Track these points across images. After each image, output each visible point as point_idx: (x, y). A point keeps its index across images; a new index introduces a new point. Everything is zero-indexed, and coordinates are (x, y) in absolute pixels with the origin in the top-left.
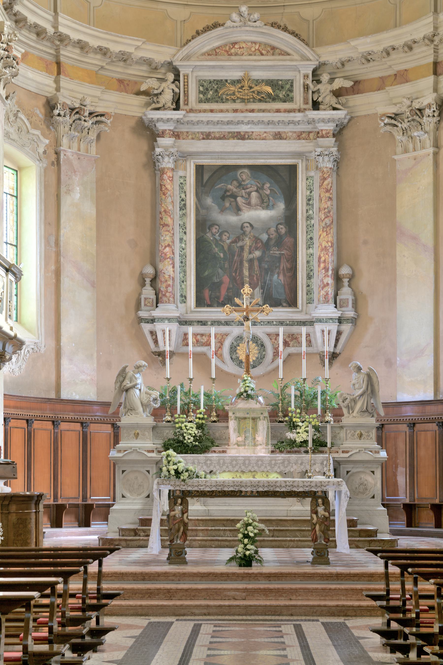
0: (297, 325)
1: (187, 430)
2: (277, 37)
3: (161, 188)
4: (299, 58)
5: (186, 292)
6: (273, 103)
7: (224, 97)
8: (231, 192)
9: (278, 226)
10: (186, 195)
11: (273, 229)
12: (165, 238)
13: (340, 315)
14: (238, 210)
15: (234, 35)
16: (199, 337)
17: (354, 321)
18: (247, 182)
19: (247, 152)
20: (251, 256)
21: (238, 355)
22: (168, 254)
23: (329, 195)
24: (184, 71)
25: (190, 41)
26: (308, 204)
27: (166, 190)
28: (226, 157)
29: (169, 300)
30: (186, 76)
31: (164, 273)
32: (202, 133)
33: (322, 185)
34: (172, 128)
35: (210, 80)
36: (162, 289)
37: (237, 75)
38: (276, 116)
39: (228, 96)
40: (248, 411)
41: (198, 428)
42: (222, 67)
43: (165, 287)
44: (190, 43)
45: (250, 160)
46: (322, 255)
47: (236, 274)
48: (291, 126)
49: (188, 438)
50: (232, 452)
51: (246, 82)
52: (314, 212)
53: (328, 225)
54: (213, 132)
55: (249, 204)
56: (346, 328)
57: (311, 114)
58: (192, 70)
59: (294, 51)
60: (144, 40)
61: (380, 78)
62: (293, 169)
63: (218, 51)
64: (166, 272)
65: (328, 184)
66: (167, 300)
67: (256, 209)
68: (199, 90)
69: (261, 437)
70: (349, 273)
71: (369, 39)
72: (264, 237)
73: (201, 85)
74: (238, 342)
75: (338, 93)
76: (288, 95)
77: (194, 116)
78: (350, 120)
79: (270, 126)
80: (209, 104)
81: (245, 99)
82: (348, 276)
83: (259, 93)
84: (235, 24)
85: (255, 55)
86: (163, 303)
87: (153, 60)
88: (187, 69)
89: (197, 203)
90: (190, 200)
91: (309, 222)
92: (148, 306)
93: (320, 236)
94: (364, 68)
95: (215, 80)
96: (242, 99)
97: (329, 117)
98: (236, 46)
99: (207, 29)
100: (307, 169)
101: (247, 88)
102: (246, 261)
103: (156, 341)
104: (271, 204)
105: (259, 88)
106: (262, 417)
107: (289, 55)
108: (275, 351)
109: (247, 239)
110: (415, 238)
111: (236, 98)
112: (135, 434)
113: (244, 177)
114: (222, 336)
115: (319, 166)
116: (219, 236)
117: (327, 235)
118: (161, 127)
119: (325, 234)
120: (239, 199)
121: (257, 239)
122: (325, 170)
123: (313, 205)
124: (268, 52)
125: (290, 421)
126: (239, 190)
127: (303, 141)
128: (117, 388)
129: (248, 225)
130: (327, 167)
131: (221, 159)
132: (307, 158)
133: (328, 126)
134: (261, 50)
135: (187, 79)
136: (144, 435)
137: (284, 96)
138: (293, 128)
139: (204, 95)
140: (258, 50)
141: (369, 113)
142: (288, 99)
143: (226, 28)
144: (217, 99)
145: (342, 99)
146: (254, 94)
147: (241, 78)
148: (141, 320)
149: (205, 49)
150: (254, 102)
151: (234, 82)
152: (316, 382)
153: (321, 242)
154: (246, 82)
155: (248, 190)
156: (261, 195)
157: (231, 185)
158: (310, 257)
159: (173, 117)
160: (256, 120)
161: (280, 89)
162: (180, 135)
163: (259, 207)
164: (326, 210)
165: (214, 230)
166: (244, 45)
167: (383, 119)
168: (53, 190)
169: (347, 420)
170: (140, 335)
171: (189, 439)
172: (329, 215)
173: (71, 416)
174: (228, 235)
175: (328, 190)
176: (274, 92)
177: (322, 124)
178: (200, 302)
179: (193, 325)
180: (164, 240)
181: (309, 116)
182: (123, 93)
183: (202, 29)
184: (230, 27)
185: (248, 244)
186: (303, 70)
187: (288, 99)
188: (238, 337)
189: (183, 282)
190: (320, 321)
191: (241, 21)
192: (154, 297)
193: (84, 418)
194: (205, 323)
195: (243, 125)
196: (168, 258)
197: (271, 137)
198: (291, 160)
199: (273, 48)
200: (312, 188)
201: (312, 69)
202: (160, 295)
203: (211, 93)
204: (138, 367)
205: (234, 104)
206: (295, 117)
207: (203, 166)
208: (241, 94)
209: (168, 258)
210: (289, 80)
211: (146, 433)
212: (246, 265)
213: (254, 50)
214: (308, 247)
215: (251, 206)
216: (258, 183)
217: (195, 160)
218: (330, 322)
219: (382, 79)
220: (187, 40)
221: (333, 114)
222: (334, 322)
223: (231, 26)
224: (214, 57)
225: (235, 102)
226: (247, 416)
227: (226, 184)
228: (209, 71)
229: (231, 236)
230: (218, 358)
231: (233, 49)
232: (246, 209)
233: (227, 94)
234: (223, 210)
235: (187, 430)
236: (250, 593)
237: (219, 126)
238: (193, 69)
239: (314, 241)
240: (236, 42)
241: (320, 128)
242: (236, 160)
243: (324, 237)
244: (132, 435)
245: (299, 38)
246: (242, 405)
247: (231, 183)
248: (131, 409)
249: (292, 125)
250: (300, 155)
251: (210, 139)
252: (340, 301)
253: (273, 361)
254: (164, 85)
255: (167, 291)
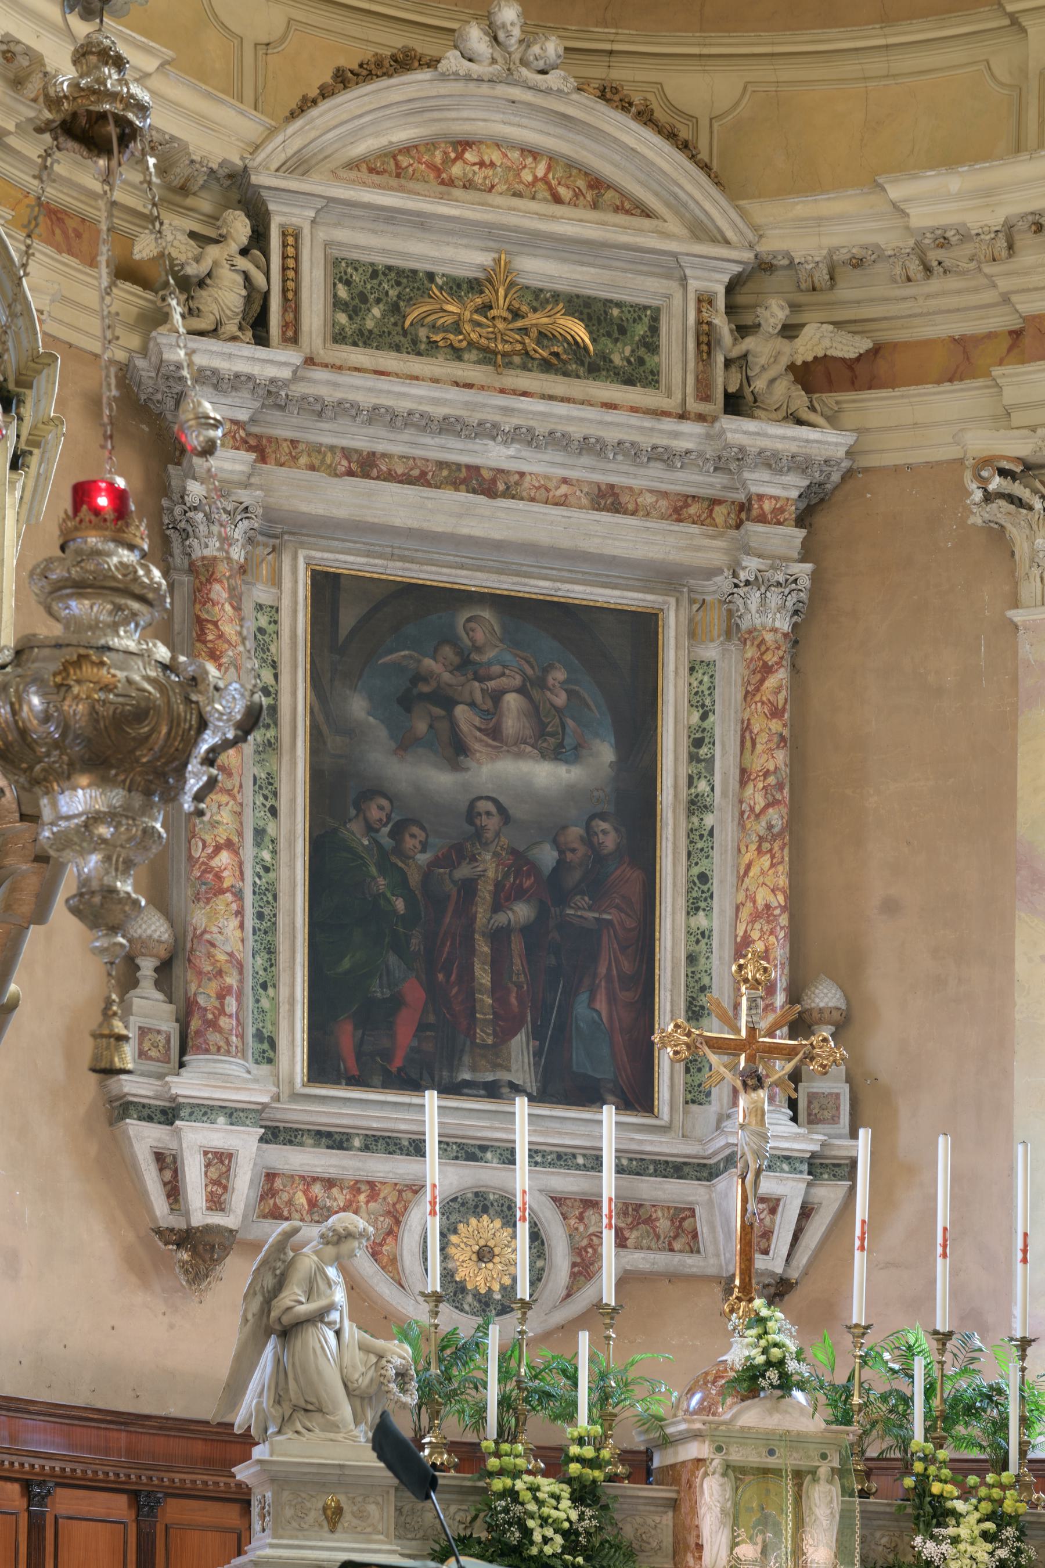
0: (655, 1174)
1: (540, 1503)
2: (616, 140)
3: (202, 632)
4: (683, 232)
5: (275, 1023)
6: (590, 382)
7: (423, 333)
8: (434, 684)
9: (594, 823)
10: (276, 676)
11: (575, 832)
12: (217, 818)
13: (816, 1148)
15: (465, 114)
16: (317, 1189)
18: (490, 654)
19: (499, 546)
20: (501, 919)
21: (450, 1266)
22: (225, 874)
23: (780, 729)
24: (285, 214)
25: (314, 102)
26: (693, 758)
27: (219, 642)
28: (420, 555)
29: (228, 1043)
30: (292, 237)
31: (213, 945)
32: (347, 453)
33: (757, 690)
34: (243, 416)
35: (372, 264)
36: (201, 1001)
38: (612, 424)
39: (437, 334)
40: (771, 1442)
41: (577, 1499)
42: (421, 222)
43: (213, 995)
44: (314, 112)
45: (503, 578)
46: (755, 935)
47: (448, 976)
48: (656, 470)
49: (544, 1537)
51: (501, 292)
53: (776, 830)
54: (384, 455)
55: (495, 733)
57: (736, 431)
58: (312, 214)
59: (668, 205)
60: (169, 54)
61: (954, 340)
63: (404, 161)
64: (218, 939)
65: (777, 691)
66: (222, 1044)
67: (519, 755)
68: (335, 295)
70: (839, 1005)
71: (954, 182)
72: (547, 856)
73: (340, 280)
74: (453, 1218)
76: (641, 361)
77: (328, 383)
78: (848, 475)
79: (586, 460)
80: (368, 351)
81: (495, 353)
82: (836, 1015)
83: (544, 337)
84: (475, 69)
85: (533, 198)
86: (207, 1051)
87: (184, 146)
88: (296, 211)
89: (316, 709)
90: (294, 693)
91: (695, 820)
92: (151, 1058)
93: (748, 867)
94: (905, 299)
95: (389, 268)
96: (485, 350)
97: (793, 448)
98: (468, 156)
100: (692, 634)
101: (505, 314)
102: (483, 935)
103: (174, 1191)
104: (568, 741)
105: (545, 320)
106: (823, 1471)
107: (648, 216)
108: (578, 1260)
109: (488, 857)
111: (465, 343)
112: (325, 1509)
113: (480, 636)
114: (400, 1192)
115: (745, 625)
116: (392, 834)
117: (772, 865)
119: (768, 864)
120: (461, 712)
122: (769, 637)
123: (710, 761)
124: (578, 194)
125: (919, 1490)
126: (463, 679)
127: (695, 529)
128: (250, 1317)
129: (490, 806)
130: (775, 630)
131: (402, 559)
132: (692, 595)
133: (784, 487)
134: (554, 183)
135: (296, 248)
136: (361, 1515)
137: (629, 362)
138: (661, 480)
139: (350, 318)
140: (545, 180)
141: (910, 461)
143: (444, 77)
144: (397, 339)
146: (527, 340)
147: (481, 275)
149: (360, 149)
150: (524, 367)
151: (459, 287)
153: (752, 888)
154: (501, 292)
155: (491, 684)
156: (536, 708)
157: (434, 659)
158: (698, 942)
159: (255, 370)
160: (541, 428)
161: (616, 335)
162: (268, 450)
163: (529, 749)
164: (772, 780)
165: (375, 813)
166: (496, 156)
167: (985, 474)
171: (546, 1540)
172: (779, 797)
174: (421, 835)
175: (776, 708)
176: (594, 341)
177: (765, 475)
179: (301, 1144)
180: (214, 824)
181: (729, 435)
182: (66, 258)
183: (355, 67)
184: (456, 77)
185: (491, 874)
186: (696, 278)
188: (455, 1200)
189: (264, 986)
191: (494, 61)
192: (170, 1027)
194: (341, 1142)
195: (491, 443)
196: (227, 890)
197: (584, 501)
198: (641, 596)
199: (597, 184)
200: (708, 702)
201: (726, 279)
202: (195, 1024)
203: (376, 312)
205: (457, 364)
206: (676, 435)
207: (337, 576)
208: (483, 331)
209: (227, 890)
210: (646, 308)
211: (372, 1508)
212: (483, 948)
213: (530, 178)
214: (693, 908)
215: (501, 741)
216: (528, 662)
217: (313, 553)
218: (782, 1171)
219: (963, 344)
220: (304, 99)
221: (808, 441)
222: (794, 1170)
223: (462, 73)
224: (394, 182)
225: (460, 359)
226: (772, 1462)
227: (416, 655)
228: (374, 232)
229: (431, 840)
230: (383, 1268)
231: (459, 164)
232: (483, 749)
233: (433, 327)
235: (540, 1503)
237: (407, 435)
238: (318, 211)
239: (715, 889)
240: (471, 139)
241: (754, 489)
242: (453, 571)
243: (763, 873)
244: (315, 1515)
245: (692, 158)
247: (436, 650)
249: (659, 465)
251: (373, 479)
252: (810, 1102)
253: (568, 1295)
254: (213, 252)
255: (222, 1011)
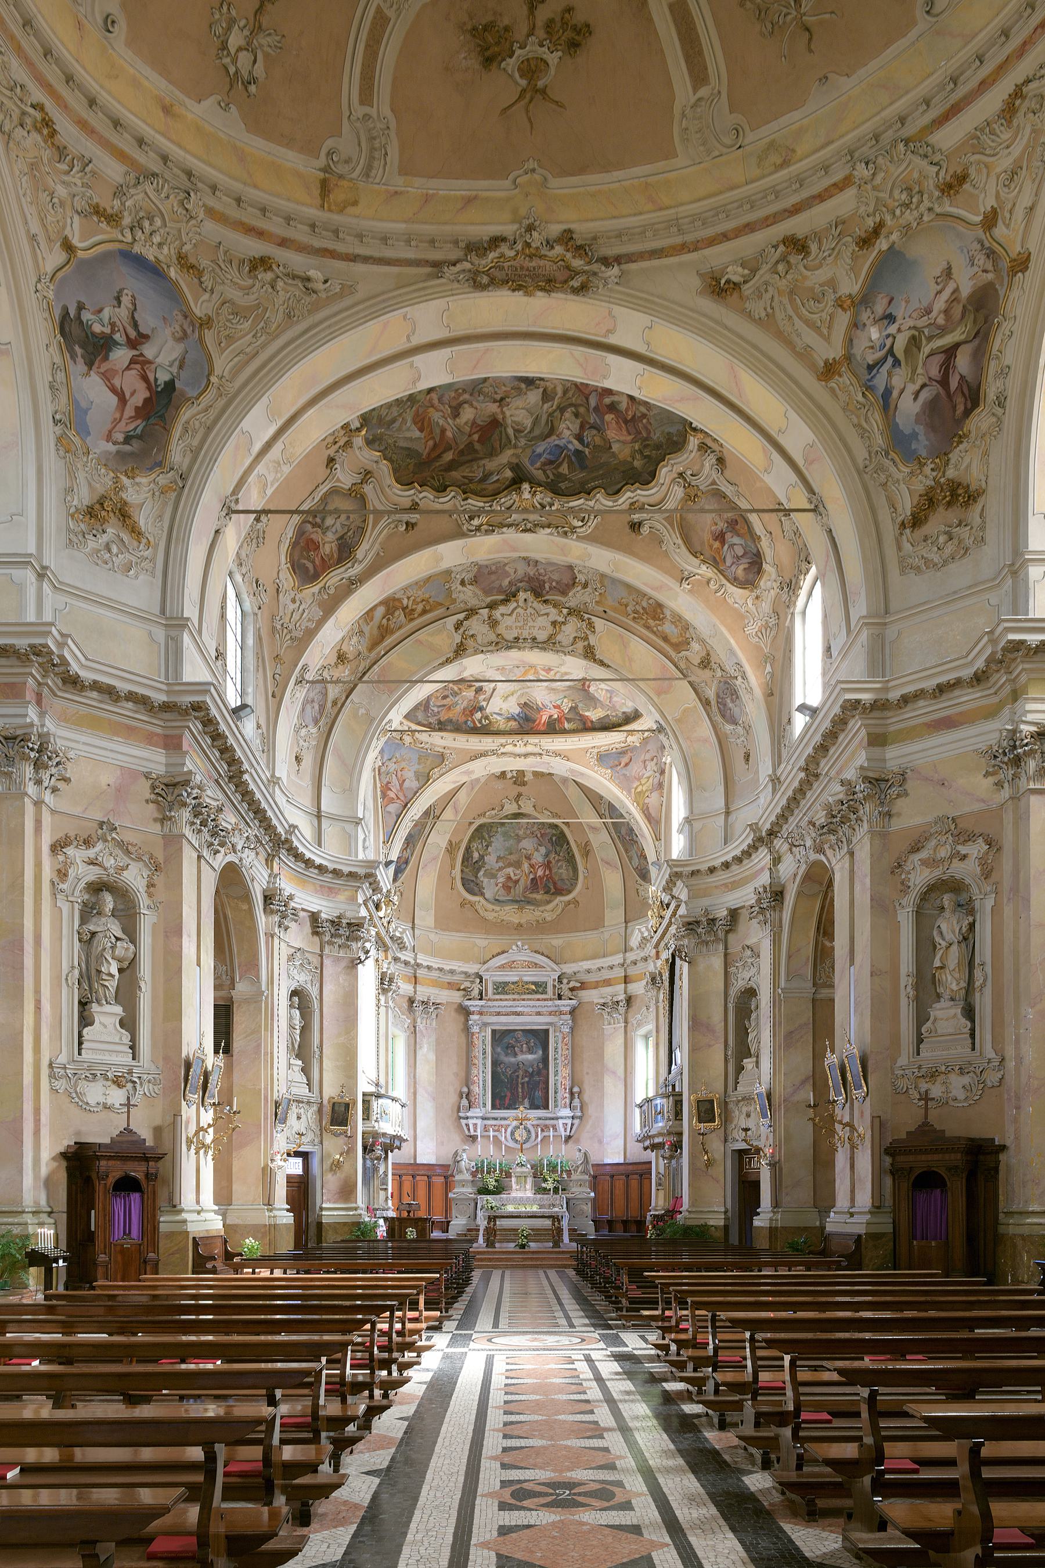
14: (515, 1055)
17: (581, 1118)
30: (486, 980)
37: (515, 979)
50: (514, 1194)
52: (559, 1056)
56: (576, 1122)
62: (547, 1031)
69: (528, 1186)
71: (589, 962)
72: (531, 1070)
75: (572, 989)
99: (499, 954)
110: (614, 1073)
118: (472, 1009)
121: (526, 1071)
142: (544, 992)
145: (575, 993)
148: (460, 1118)
151: (513, 983)
152: (558, 1156)
168: (412, 1048)
169: (574, 1177)
170: (460, 1126)
173: (422, 1172)
178: (494, 1107)
187: (544, 992)
190: (562, 1118)
193: (429, 1173)
204: (464, 1150)
234: (507, 1055)
236: (525, 1259)
246: (519, 1169)
248: (460, 1172)
250: (551, 1024)
